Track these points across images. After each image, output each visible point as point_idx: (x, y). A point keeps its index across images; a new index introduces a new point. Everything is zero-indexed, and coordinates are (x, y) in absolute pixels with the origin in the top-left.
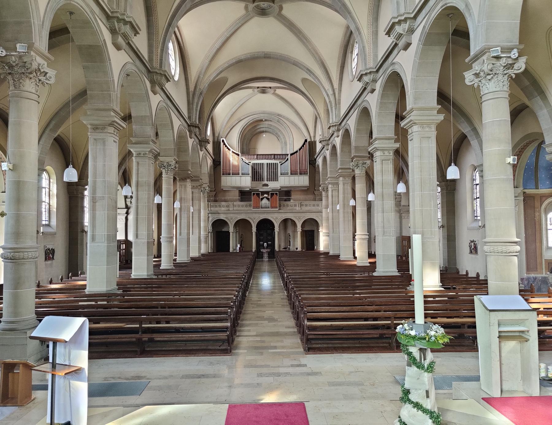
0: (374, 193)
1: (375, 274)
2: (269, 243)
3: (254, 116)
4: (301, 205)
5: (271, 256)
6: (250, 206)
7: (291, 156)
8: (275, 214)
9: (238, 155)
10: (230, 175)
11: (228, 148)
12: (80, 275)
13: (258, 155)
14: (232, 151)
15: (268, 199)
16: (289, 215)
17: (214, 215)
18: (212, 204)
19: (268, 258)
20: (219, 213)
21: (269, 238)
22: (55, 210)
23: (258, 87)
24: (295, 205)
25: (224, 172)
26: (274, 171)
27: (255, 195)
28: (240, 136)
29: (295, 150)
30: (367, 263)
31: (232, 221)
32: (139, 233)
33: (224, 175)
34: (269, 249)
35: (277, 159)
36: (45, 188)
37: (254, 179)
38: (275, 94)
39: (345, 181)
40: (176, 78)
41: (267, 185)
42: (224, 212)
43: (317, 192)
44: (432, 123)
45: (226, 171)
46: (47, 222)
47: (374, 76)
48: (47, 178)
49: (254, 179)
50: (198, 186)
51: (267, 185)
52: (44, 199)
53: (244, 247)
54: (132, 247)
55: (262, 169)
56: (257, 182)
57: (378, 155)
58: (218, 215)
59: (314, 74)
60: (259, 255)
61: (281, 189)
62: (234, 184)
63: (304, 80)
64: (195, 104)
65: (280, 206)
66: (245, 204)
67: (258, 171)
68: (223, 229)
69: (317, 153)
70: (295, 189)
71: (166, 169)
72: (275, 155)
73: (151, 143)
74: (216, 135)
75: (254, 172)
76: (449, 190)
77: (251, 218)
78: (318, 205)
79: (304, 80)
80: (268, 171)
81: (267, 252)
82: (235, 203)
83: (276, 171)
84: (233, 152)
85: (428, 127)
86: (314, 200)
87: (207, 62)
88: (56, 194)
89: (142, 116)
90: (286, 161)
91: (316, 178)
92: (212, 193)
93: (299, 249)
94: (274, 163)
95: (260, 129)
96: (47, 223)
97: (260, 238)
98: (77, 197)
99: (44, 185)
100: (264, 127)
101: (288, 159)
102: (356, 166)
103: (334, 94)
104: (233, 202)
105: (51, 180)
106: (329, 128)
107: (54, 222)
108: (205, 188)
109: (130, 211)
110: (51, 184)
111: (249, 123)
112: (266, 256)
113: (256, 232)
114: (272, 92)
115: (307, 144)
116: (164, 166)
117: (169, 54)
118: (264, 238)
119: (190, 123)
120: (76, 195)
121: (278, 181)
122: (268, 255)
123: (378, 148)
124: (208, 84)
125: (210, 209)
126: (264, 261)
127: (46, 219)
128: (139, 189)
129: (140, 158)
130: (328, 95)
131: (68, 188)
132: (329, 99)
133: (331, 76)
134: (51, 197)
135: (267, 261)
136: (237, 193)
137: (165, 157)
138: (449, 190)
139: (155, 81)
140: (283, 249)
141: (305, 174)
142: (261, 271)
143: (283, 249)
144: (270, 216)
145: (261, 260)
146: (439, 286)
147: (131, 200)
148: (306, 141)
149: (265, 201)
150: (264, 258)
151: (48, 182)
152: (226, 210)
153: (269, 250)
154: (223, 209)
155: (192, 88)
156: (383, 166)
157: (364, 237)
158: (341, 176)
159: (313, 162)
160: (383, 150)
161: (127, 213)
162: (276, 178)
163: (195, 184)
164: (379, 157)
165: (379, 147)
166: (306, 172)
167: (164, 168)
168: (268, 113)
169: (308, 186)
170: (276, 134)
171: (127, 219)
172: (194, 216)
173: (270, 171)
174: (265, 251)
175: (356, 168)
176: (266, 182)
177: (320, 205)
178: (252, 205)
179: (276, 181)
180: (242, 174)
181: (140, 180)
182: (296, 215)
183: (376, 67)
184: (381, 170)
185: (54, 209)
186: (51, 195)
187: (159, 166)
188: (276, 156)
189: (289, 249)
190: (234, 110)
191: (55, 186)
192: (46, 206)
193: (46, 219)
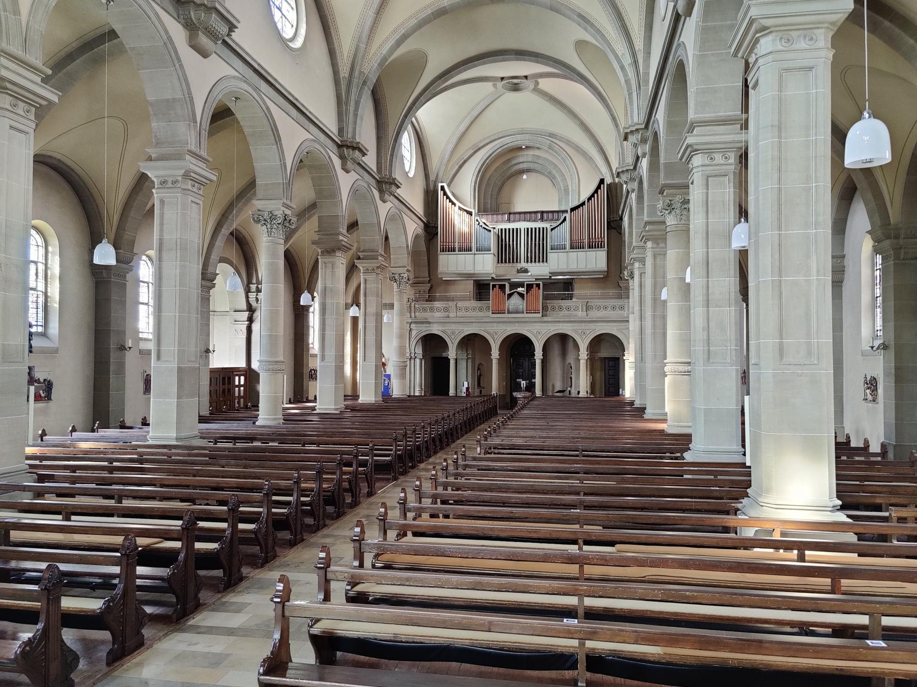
1: (689, 457)
3: (503, 139)
4: (588, 308)
8: (536, 324)
9: (470, 213)
11: (451, 201)
12: (97, 428)
13: (510, 214)
15: (521, 295)
16: (564, 328)
18: (417, 306)
20: (429, 323)
22: (57, 306)
23: (502, 79)
24: (576, 309)
28: (476, 179)
29: (582, 200)
32: (163, 348)
33: (443, 251)
35: (547, 220)
36: (36, 263)
38: (536, 90)
39: (656, 250)
41: (526, 271)
42: (439, 321)
44: (817, 25)
45: (447, 244)
46: (150, 334)
48: (40, 244)
50: (375, 268)
51: (526, 271)
53: (484, 388)
54: (259, 383)
56: (507, 264)
58: (427, 325)
59: (592, 25)
61: (553, 278)
62: (462, 269)
63: (580, 45)
64: (352, 103)
65: (545, 308)
67: (509, 245)
68: (444, 354)
70: (579, 277)
71: (269, 226)
72: (542, 212)
73: (188, 157)
74: (432, 178)
76: (903, 259)
77: (488, 333)
79: (580, 45)
80: (528, 244)
82: (460, 304)
83: (543, 244)
84: (460, 208)
85: (805, 37)
86: (618, 298)
87: (371, 14)
88: (58, 275)
89: (168, 100)
90: (562, 223)
92: (424, 286)
94: (539, 228)
95: (516, 166)
96: (40, 329)
98: (109, 282)
99: (33, 256)
100: (525, 160)
101: (565, 219)
102: (667, 208)
103: (635, 62)
104: (455, 303)
105: (50, 249)
106: (626, 139)
107: (54, 328)
108: (403, 275)
109: (255, 315)
110: (50, 255)
111: (495, 154)
113: (499, 359)
114: (531, 86)
115: (604, 188)
116: (265, 220)
119: (341, 141)
120: (107, 278)
121: (546, 261)
123: (695, 147)
124: (379, 61)
125: (413, 314)
127: (37, 321)
128: (164, 254)
129: (166, 190)
130: (622, 68)
132: (625, 75)
133: (628, 24)
134: (49, 280)
136: (470, 286)
137: (267, 202)
138: (903, 259)
139: (194, 24)
144: (526, 329)
146: (830, 509)
147: (257, 295)
148: (602, 181)
149: (515, 300)
151: (42, 251)
152: (442, 316)
154: (437, 314)
155: (344, 72)
156: (710, 191)
158: (648, 240)
159: (614, 225)
160: (709, 151)
161: (251, 320)
162: (543, 258)
163: (369, 265)
164: (700, 169)
165: (697, 144)
166: (601, 244)
167: (265, 224)
168: (531, 132)
169: (604, 272)
170: (550, 173)
171: (249, 330)
172: (367, 327)
173: (532, 244)
174: (519, 396)
175: (667, 212)
176: (523, 264)
177: (626, 307)
179: (543, 261)
181: (166, 237)
182: (576, 327)
184: (705, 200)
185: (55, 305)
186: (49, 277)
187: (254, 219)
188: (545, 215)
189: (570, 394)
190: (462, 128)
191: (57, 259)
192: (37, 297)
193: (37, 321)
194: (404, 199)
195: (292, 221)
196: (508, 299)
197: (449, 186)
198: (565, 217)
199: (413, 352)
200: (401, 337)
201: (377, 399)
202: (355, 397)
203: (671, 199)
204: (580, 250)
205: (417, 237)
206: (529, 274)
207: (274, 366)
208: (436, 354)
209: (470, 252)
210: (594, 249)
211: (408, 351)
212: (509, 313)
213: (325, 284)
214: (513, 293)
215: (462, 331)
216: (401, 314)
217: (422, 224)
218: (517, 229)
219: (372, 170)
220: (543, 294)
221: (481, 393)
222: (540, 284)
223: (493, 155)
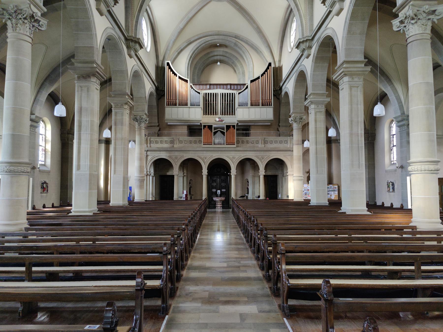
0: (308, 141)
2: (223, 190)
4: (265, 142)
5: (225, 205)
6: (200, 142)
7: (251, 83)
8: (232, 152)
9: (186, 81)
10: (176, 105)
13: (210, 85)
14: (179, 77)
17: (154, 152)
18: (151, 140)
19: (221, 208)
21: (223, 184)
24: (257, 142)
25: (168, 102)
26: (230, 104)
27: (206, 127)
29: (256, 77)
30: (302, 199)
31: (176, 161)
33: (168, 105)
34: (223, 197)
36: (42, 135)
37: (206, 112)
39: (351, 83)
40: (148, 50)
43: (283, 129)
46: (43, 162)
47: (310, 43)
49: (206, 112)
52: (41, 144)
53: (193, 195)
55: (216, 100)
57: (312, 108)
58: (159, 152)
60: (211, 204)
65: (238, 142)
66: (194, 140)
67: (211, 104)
68: (168, 173)
69: (283, 79)
72: (231, 85)
75: (206, 103)
78: (286, 142)
80: (223, 103)
81: (221, 201)
83: (232, 104)
90: (245, 89)
91: (281, 112)
93: (262, 197)
96: (43, 163)
97: (213, 184)
98: (68, 143)
100: (219, 54)
111: (201, 47)
112: (219, 205)
117: (143, 30)
118: (217, 184)
121: (234, 114)
122: (222, 204)
125: (149, 145)
126: (218, 212)
131: (61, 136)
135: (221, 212)
140: (241, 197)
141: (268, 105)
142: (211, 228)
143: (241, 197)
144: (225, 155)
145: (213, 210)
148: (270, 64)
150: (217, 208)
153: (223, 199)
157: (300, 178)
158: (345, 75)
162: (232, 112)
174: (217, 200)
178: (202, 141)
180: (191, 105)
183: (311, 36)
187: (133, 119)
194: (144, 62)
195: (41, 23)
196: (214, 135)
197: (172, 63)
198: (247, 86)
199: (148, 170)
200: (141, 159)
201: (125, 203)
202: (107, 202)
203: (418, 9)
204: (256, 107)
205: (151, 94)
206: (224, 122)
207: (16, 168)
208: (162, 173)
209: (186, 106)
210: (265, 106)
211: (145, 170)
212: (214, 144)
213: (81, 105)
214: (217, 131)
215: (182, 157)
216: (141, 144)
217: (154, 87)
218: (216, 94)
219: (122, 26)
220: (237, 133)
221: (191, 198)
222: (235, 125)
223: (200, 48)
